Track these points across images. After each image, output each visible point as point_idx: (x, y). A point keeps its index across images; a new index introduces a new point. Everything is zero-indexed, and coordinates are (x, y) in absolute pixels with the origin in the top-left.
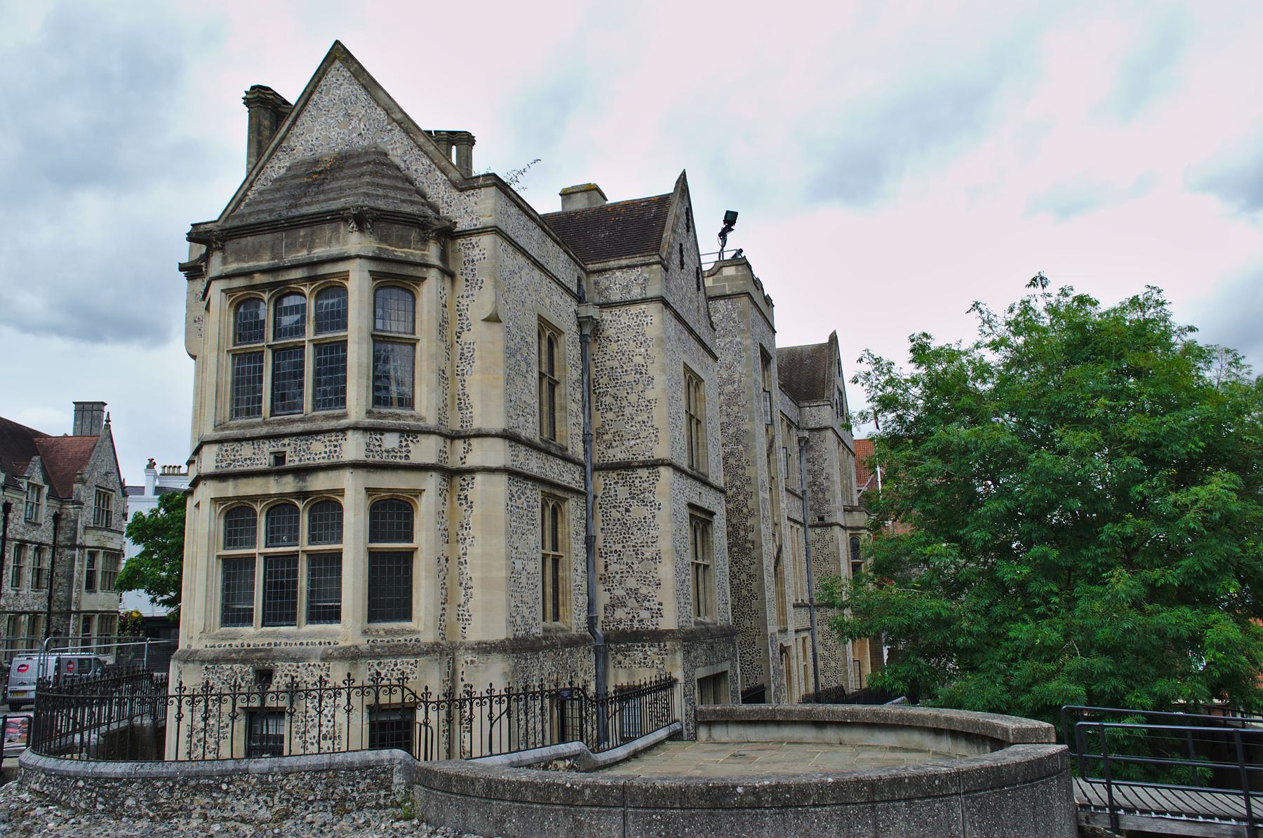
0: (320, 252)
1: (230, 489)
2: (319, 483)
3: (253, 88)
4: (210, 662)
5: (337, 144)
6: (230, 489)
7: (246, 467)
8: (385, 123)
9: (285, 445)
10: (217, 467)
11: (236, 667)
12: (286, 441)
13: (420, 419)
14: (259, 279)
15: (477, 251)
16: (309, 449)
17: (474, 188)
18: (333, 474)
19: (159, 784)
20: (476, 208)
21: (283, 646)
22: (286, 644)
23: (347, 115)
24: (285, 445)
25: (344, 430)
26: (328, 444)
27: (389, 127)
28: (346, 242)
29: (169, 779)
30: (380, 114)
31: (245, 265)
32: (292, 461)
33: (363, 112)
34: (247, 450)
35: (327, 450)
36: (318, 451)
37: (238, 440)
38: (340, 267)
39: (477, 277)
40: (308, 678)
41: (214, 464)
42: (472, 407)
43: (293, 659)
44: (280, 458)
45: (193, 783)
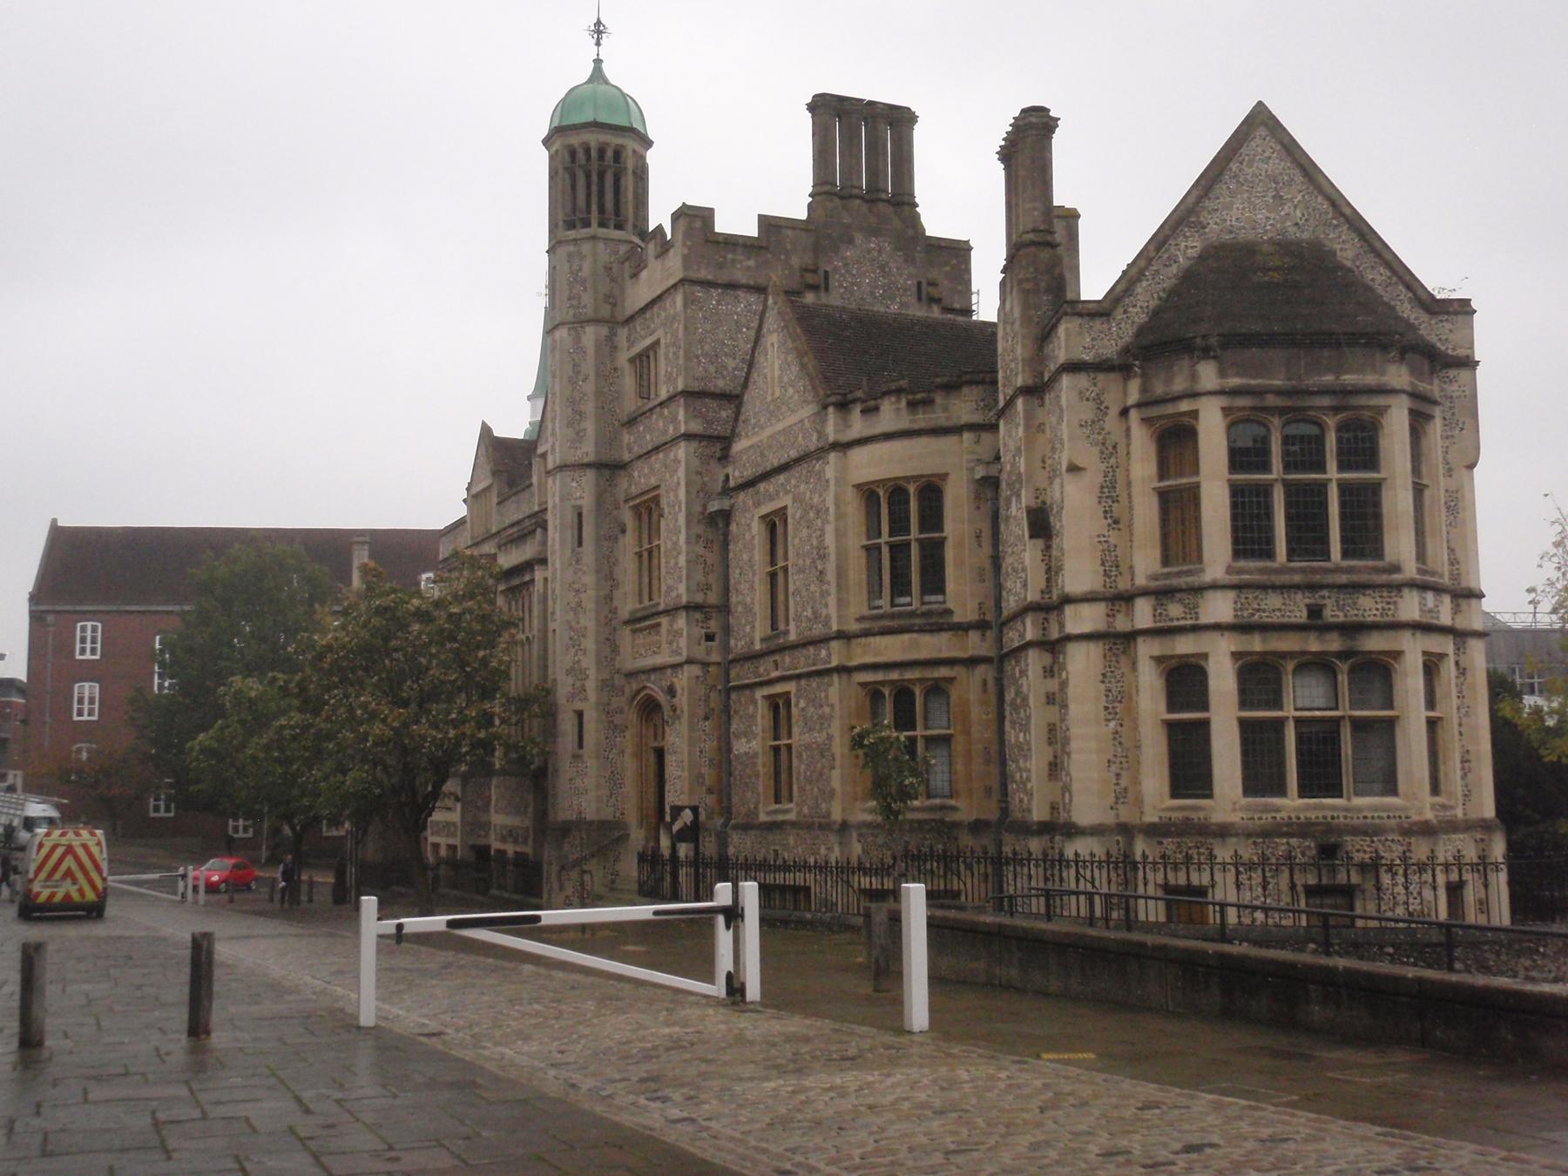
0: (1349, 379)
1: (1256, 644)
2: (1374, 643)
3: (1023, 111)
4: (1259, 835)
5: (1266, 231)
6: (1256, 644)
7: (1276, 619)
8: (1330, 216)
9: (1323, 597)
10: (1236, 616)
11: (1294, 841)
12: (1325, 593)
13: (1433, 574)
14: (1271, 400)
15: (1455, 387)
16: (1355, 603)
17: (1448, 313)
18: (1391, 634)
19: (1486, 947)
20: (1451, 336)
21: (1342, 820)
22: (1345, 817)
23: (1278, 197)
24: (1323, 597)
25: (1399, 587)
26: (1379, 600)
27: (1335, 222)
28: (1383, 373)
29: (1495, 943)
30: (1322, 204)
31: (1253, 382)
32: (1332, 614)
33: (1299, 197)
34: (1274, 601)
35: (1379, 606)
36: (1368, 607)
37: (1264, 587)
38: (1380, 401)
39: (1457, 417)
40: (1391, 852)
41: (1232, 613)
42: (1458, 563)
43: (1365, 833)
44: (1315, 612)
45: (1517, 946)
